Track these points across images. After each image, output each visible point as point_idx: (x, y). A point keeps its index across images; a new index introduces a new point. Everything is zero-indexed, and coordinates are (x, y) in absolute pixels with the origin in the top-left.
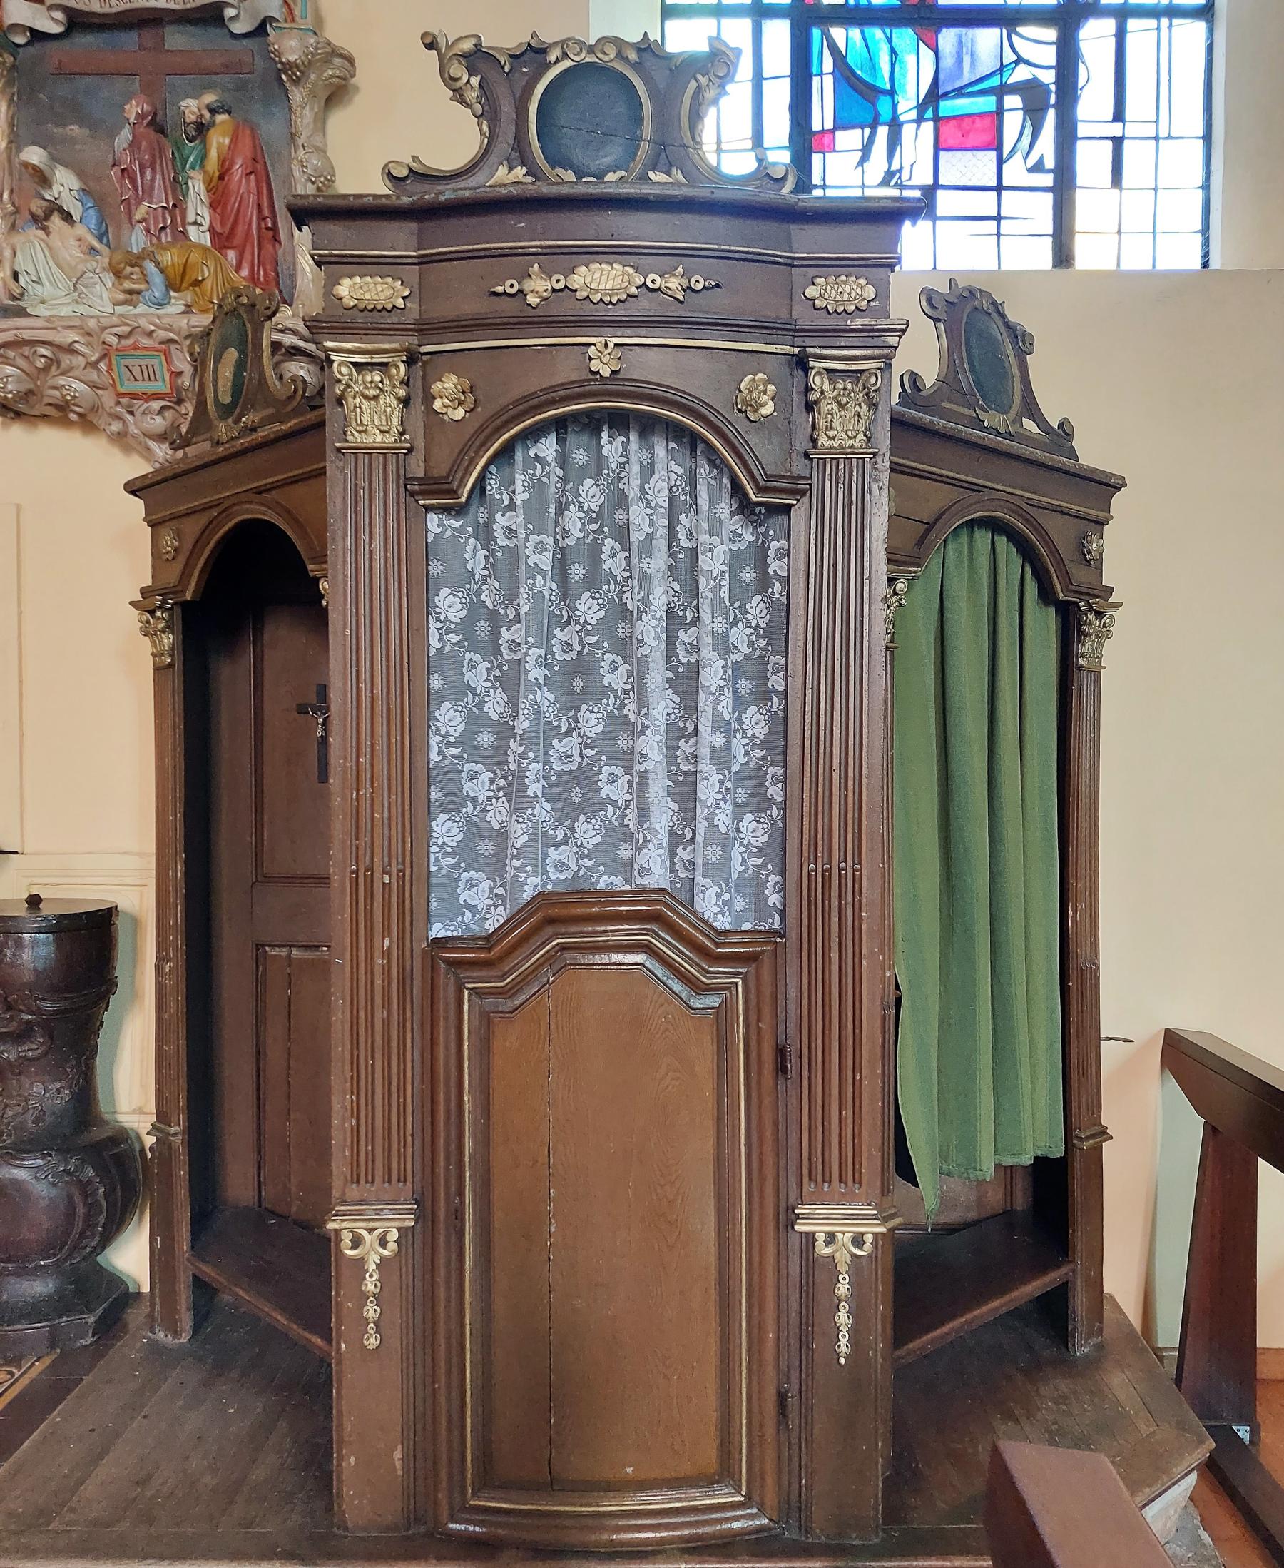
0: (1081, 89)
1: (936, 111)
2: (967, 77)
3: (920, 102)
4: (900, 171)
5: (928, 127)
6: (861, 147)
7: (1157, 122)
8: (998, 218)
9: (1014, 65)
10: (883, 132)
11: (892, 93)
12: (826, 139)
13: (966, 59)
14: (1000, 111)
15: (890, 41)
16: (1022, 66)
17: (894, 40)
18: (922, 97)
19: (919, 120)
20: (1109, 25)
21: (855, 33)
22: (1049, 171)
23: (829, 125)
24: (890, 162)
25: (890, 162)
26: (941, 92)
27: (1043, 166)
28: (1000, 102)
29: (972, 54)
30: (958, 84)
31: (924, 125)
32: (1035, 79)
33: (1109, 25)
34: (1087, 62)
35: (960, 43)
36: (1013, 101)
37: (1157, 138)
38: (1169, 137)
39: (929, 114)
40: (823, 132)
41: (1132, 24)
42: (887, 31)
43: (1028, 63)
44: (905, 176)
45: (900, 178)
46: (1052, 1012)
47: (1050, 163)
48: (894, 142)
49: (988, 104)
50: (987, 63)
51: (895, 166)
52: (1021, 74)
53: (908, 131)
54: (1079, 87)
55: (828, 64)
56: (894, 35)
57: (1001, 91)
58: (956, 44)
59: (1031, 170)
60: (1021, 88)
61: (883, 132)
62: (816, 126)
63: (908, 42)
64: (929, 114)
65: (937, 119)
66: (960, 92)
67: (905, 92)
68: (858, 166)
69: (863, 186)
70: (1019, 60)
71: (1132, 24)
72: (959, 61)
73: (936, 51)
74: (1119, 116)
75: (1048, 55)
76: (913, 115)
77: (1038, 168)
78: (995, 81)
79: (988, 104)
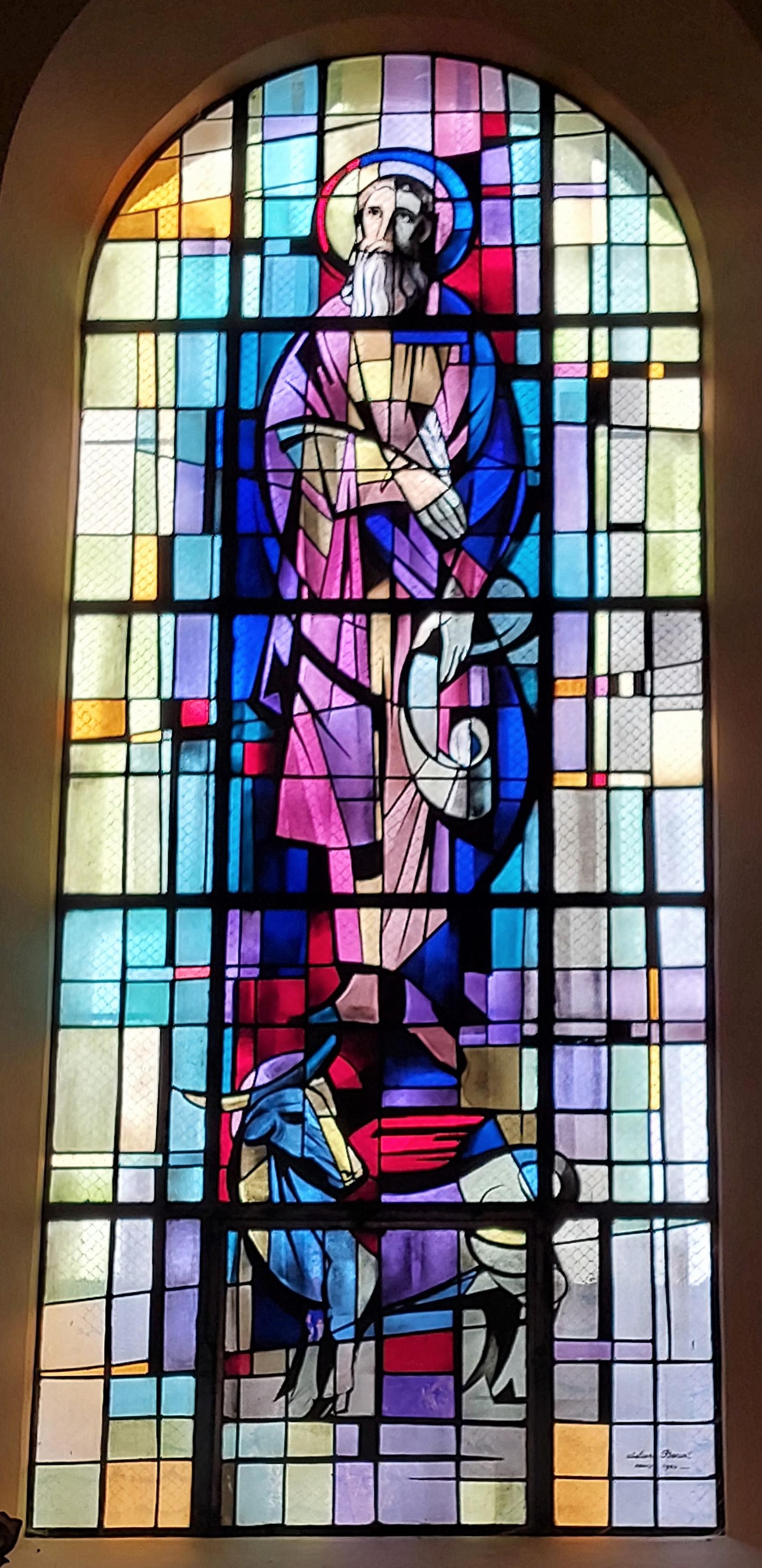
0: (560, 1300)
1: (379, 1328)
2: (417, 1286)
3: (359, 1316)
4: (335, 1397)
5: (368, 1347)
6: (283, 1371)
7: (653, 1341)
8: (458, 1459)
9: (474, 1273)
10: (312, 1354)
11: (325, 1306)
12: (244, 1360)
13: (416, 1266)
14: (457, 1329)
15: (322, 1244)
16: (485, 1275)
17: (328, 1244)
18: (360, 1311)
19: (357, 1341)
20: (591, 1226)
21: (280, 1236)
22: (520, 1401)
23: (245, 1345)
24: (321, 1387)
25: (321, 1387)
26: (384, 1303)
27: (513, 1393)
28: (458, 1319)
29: (423, 1260)
30: (407, 1295)
31: (363, 1345)
32: (500, 1289)
33: (591, 1226)
34: (565, 1268)
35: (408, 1246)
36: (475, 1317)
37: (655, 1362)
38: (669, 1361)
39: (370, 1331)
40: (238, 1352)
41: (618, 1225)
42: (319, 1233)
43: (492, 1270)
44: (340, 1404)
45: (334, 1408)
46: (363, 1277)
47: (520, 1391)
48: (326, 1365)
49: (442, 1319)
50: (440, 1272)
51: (328, 1392)
52: (483, 1283)
53: (344, 1351)
54: (556, 1298)
55: (246, 1274)
56: (327, 1239)
57: (460, 1304)
58: (403, 1249)
59: (497, 1399)
60: (481, 1300)
61: (312, 1354)
62: (230, 1347)
63: (344, 1245)
64: (370, 1331)
65: (379, 1339)
66: (409, 1306)
67: (339, 1304)
68: (279, 1396)
69: (649, 1111)
70: (482, 1268)
71: (618, 1225)
72: (408, 1269)
73: (378, 1255)
74: (606, 1331)
75: (517, 1262)
76: (350, 1333)
77: (507, 1396)
78: (451, 1292)
79: (442, 1319)
